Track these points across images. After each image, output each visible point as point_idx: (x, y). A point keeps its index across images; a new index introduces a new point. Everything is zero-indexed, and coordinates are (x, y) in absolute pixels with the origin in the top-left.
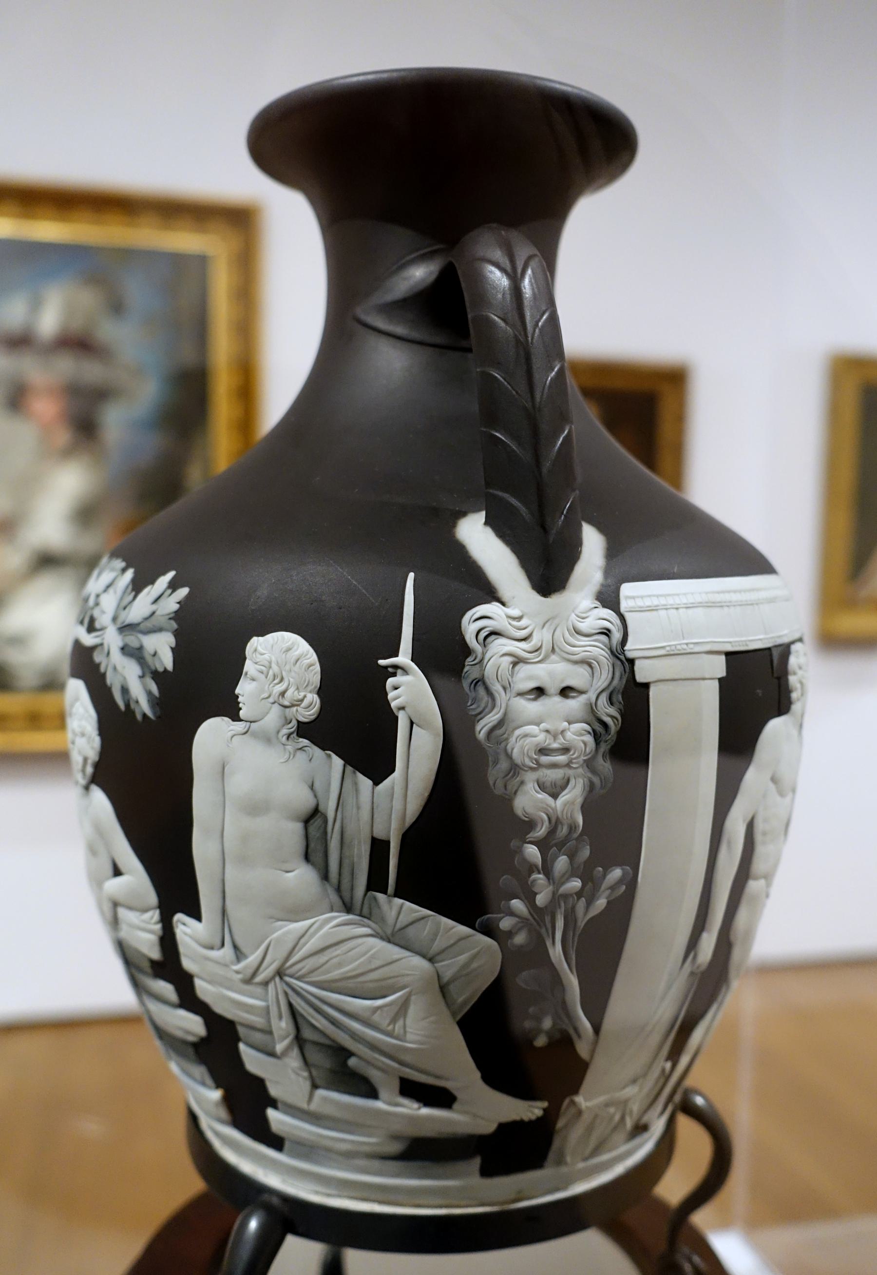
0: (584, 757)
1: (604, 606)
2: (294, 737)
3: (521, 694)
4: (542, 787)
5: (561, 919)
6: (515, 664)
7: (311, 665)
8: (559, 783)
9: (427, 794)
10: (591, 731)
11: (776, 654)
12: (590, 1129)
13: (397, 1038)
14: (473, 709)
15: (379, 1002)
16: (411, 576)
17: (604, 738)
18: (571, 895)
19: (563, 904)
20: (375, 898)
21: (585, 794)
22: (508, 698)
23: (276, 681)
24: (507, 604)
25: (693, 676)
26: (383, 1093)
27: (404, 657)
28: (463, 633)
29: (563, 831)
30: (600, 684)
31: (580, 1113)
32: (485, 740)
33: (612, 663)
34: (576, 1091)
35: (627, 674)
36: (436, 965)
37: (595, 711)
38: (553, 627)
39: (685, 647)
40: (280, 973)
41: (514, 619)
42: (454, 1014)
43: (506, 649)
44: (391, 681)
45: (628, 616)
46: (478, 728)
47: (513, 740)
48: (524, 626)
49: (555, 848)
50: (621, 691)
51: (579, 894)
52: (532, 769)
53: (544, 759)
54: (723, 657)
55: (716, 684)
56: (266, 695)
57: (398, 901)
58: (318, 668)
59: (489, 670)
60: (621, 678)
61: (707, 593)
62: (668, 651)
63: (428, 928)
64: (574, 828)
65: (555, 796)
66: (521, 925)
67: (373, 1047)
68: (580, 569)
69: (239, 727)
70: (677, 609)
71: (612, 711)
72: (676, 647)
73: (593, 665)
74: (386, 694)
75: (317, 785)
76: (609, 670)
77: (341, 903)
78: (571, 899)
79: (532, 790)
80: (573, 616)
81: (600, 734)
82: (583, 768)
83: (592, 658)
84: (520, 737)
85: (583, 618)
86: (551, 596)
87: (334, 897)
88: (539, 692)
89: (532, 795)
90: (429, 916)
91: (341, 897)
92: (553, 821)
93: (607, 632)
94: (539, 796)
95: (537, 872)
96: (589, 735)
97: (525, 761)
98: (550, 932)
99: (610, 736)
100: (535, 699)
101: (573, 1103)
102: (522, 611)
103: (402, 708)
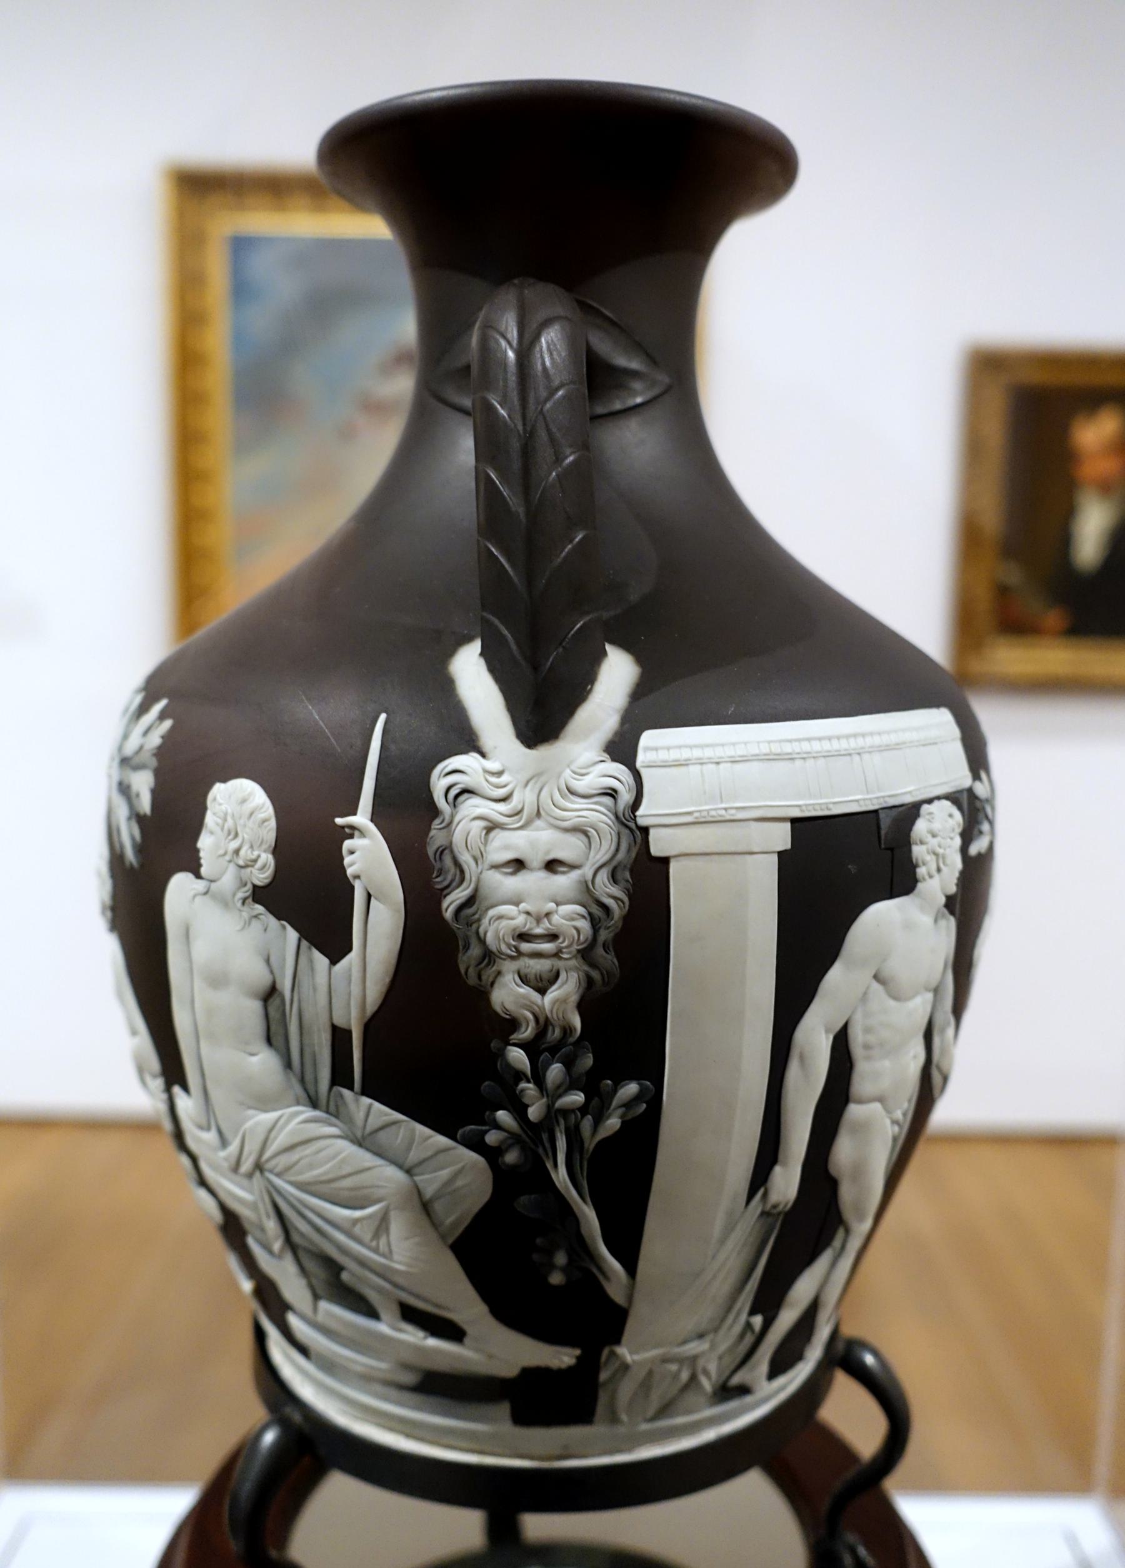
0: (578, 945)
1: (614, 760)
2: (249, 903)
3: (495, 867)
4: (524, 980)
5: (562, 1139)
6: (489, 830)
7: (264, 821)
8: (545, 976)
9: (388, 980)
10: (586, 915)
11: (885, 822)
12: (646, 1385)
13: (383, 1255)
14: (439, 882)
15: (358, 1214)
16: (383, 717)
17: (605, 924)
18: (573, 1111)
19: (562, 1122)
20: (341, 1096)
21: (581, 990)
22: (479, 870)
23: (230, 837)
24: (489, 755)
25: (733, 849)
26: (383, 1315)
27: (362, 818)
28: (432, 790)
29: (555, 1034)
30: (598, 857)
31: (625, 1367)
32: (453, 921)
33: (617, 832)
34: (618, 1341)
35: (638, 845)
36: (417, 1178)
37: (592, 891)
38: (538, 786)
39: (723, 812)
40: (259, 1167)
41: (493, 774)
42: (443, 1237)
43: (478, 811)
44: (347, 844)
45: (644, 773)
46: (445, 904)
47: (485, 922)
48: (503, 784)
49: (547, 1053)
50: (629, 866)
51: (584, 1109)
52: (512, 958)
53: (525, 947)
54: (788, 825)
55: (775, 858)
56: (221, 852)
57: (366, 1101)
58: (273, 823)
59: (458, 837)
60: (629, 850)
61: (769, 742)
62: (696, 818)
63: (401, 1135)
64: (568, 1031)
65: (542, 991)
66: (510, 1141)
67: (362, 1263)
68: (585, 714)
69: (200, 885)
70: (718, 763)
71: (615, 891)
72: (708, 813)
73: (590, 834)
74: (342, 859)
75: (273, 959)
76: (612, 839)
77: (305, 1096)
78: (573, 1116)
79: (511, 983)
80: (568, 772)
81: (600, 919)
82: (576, 958)
83: (589, 825)
84: (494, 918)
85: (582, 775)
86: (537, 747)
87: (298, 1089)
88: (518, 865)
89: (512, 989)
90: (403, 1121)
91: (306, 1090)
92: (542, 1020)
93: (612, 793)
94: (521, 990)
95: (525, 1079)
96: (584, 920)
97: (502, 947)
98: (550, 1154)
99: (613, 922)
100: (514, 873)
101: (613, 1354)
102: (503, 765)
103: (357, 877)
